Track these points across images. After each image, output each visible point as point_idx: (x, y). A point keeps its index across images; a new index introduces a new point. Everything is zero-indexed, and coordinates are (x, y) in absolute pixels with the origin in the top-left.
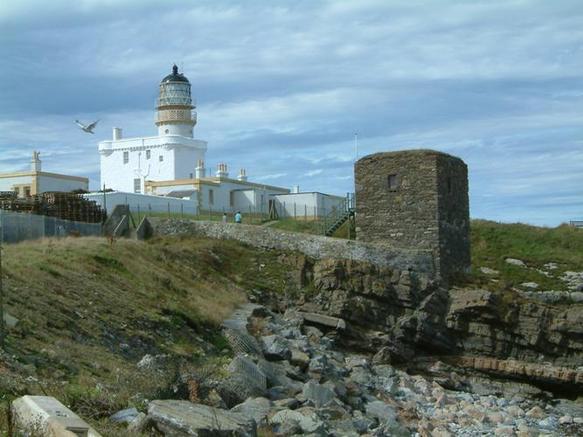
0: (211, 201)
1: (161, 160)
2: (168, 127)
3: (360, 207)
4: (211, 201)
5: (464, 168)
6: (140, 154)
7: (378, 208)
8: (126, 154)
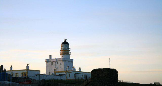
0: (69, 76)
3: (92, 81)
4: (69, 76)
5: (117, 72)
6: (56, 63)
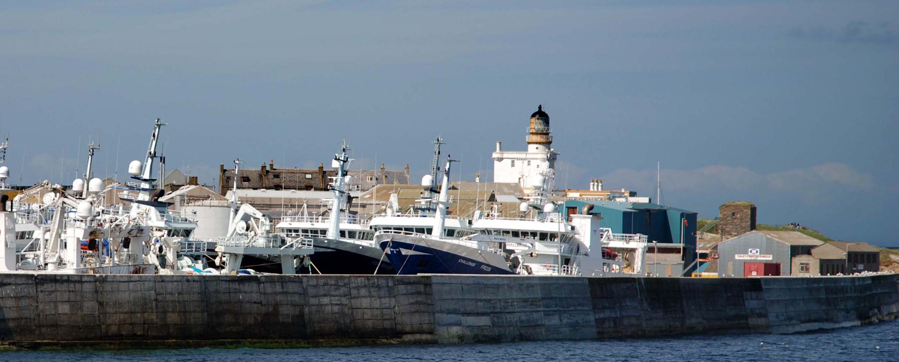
1: (538, 166)
2: (537, 146)
7: (728, 224)
8: (513, 162)
